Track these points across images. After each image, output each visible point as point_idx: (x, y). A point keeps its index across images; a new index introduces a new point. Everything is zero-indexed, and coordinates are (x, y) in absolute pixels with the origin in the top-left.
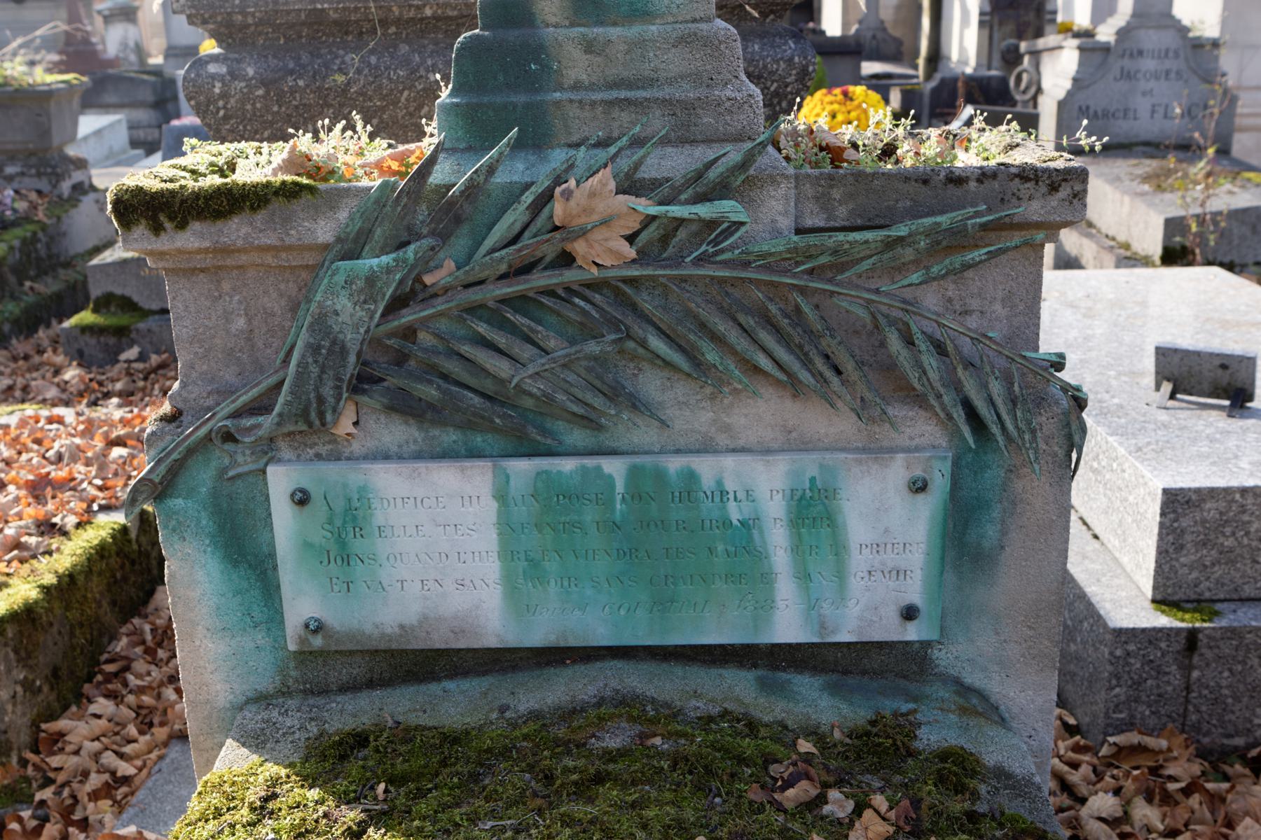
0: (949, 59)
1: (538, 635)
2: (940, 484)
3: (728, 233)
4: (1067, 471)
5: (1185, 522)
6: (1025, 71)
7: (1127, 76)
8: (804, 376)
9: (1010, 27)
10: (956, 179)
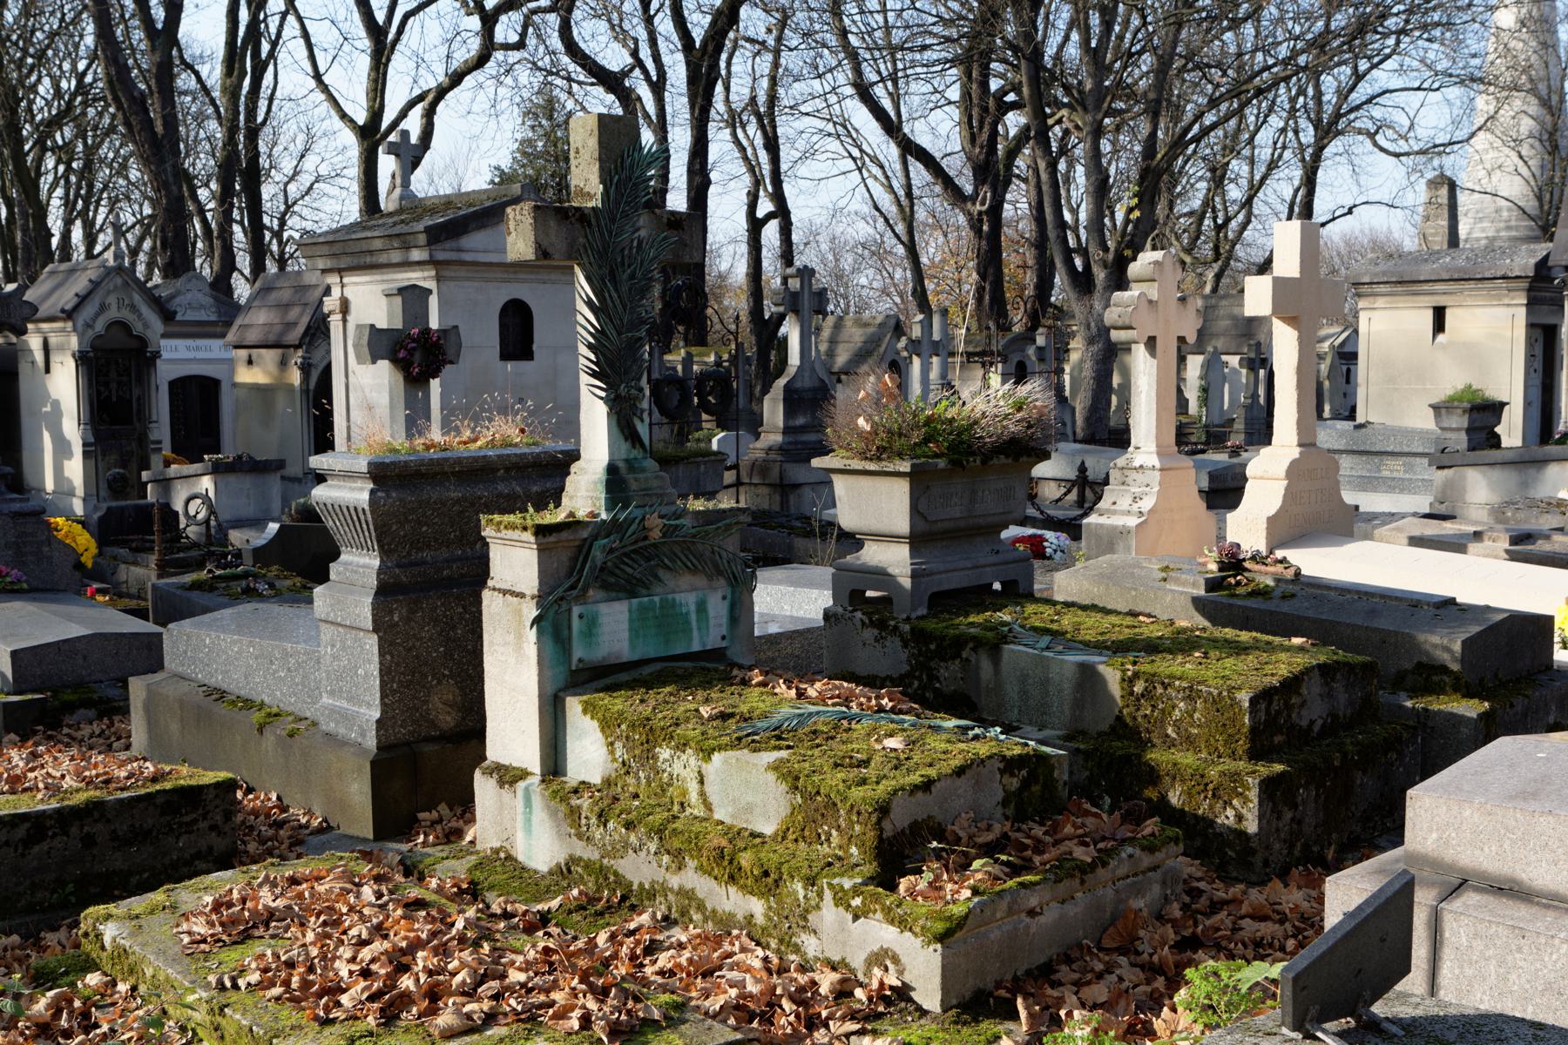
1: (636, 657)
2: (729, 596)
9: (113, 458)
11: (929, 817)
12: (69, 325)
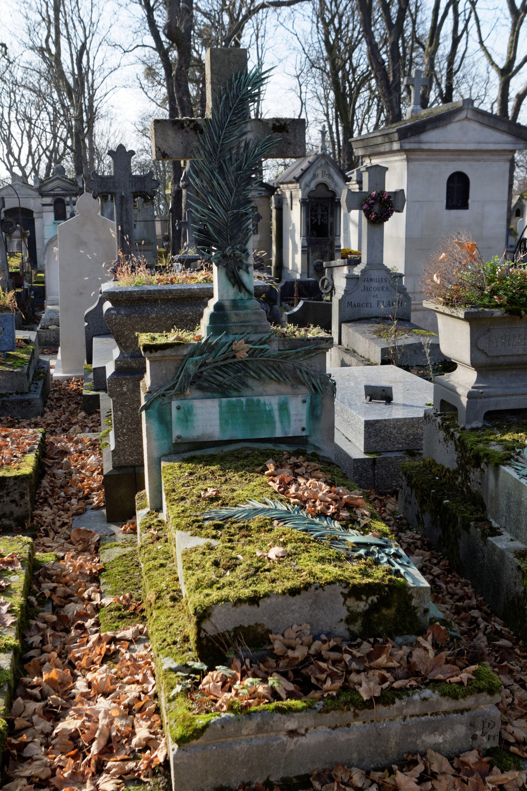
0: (288, 269)
1: (226, 438)
2: (308, 401)
3: (266, 351)
4: (333, 398)
5: (371, 430)
6: (326, 279)
7: (367, 289)
8: (281, 379)
9: (317, 254)
10: (309, 340)
11: (257, 624)
12: (298, 185)
